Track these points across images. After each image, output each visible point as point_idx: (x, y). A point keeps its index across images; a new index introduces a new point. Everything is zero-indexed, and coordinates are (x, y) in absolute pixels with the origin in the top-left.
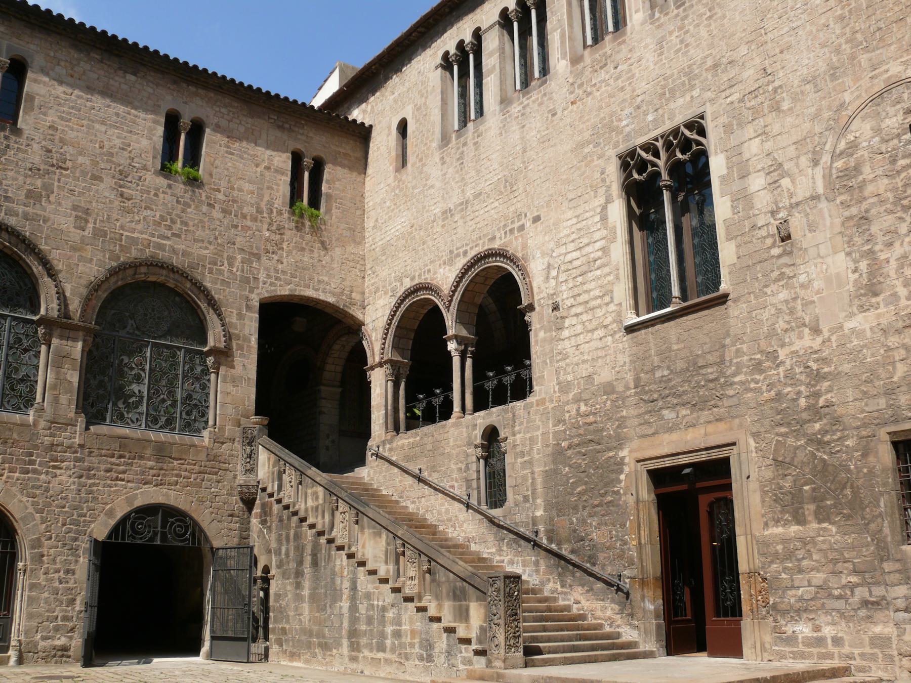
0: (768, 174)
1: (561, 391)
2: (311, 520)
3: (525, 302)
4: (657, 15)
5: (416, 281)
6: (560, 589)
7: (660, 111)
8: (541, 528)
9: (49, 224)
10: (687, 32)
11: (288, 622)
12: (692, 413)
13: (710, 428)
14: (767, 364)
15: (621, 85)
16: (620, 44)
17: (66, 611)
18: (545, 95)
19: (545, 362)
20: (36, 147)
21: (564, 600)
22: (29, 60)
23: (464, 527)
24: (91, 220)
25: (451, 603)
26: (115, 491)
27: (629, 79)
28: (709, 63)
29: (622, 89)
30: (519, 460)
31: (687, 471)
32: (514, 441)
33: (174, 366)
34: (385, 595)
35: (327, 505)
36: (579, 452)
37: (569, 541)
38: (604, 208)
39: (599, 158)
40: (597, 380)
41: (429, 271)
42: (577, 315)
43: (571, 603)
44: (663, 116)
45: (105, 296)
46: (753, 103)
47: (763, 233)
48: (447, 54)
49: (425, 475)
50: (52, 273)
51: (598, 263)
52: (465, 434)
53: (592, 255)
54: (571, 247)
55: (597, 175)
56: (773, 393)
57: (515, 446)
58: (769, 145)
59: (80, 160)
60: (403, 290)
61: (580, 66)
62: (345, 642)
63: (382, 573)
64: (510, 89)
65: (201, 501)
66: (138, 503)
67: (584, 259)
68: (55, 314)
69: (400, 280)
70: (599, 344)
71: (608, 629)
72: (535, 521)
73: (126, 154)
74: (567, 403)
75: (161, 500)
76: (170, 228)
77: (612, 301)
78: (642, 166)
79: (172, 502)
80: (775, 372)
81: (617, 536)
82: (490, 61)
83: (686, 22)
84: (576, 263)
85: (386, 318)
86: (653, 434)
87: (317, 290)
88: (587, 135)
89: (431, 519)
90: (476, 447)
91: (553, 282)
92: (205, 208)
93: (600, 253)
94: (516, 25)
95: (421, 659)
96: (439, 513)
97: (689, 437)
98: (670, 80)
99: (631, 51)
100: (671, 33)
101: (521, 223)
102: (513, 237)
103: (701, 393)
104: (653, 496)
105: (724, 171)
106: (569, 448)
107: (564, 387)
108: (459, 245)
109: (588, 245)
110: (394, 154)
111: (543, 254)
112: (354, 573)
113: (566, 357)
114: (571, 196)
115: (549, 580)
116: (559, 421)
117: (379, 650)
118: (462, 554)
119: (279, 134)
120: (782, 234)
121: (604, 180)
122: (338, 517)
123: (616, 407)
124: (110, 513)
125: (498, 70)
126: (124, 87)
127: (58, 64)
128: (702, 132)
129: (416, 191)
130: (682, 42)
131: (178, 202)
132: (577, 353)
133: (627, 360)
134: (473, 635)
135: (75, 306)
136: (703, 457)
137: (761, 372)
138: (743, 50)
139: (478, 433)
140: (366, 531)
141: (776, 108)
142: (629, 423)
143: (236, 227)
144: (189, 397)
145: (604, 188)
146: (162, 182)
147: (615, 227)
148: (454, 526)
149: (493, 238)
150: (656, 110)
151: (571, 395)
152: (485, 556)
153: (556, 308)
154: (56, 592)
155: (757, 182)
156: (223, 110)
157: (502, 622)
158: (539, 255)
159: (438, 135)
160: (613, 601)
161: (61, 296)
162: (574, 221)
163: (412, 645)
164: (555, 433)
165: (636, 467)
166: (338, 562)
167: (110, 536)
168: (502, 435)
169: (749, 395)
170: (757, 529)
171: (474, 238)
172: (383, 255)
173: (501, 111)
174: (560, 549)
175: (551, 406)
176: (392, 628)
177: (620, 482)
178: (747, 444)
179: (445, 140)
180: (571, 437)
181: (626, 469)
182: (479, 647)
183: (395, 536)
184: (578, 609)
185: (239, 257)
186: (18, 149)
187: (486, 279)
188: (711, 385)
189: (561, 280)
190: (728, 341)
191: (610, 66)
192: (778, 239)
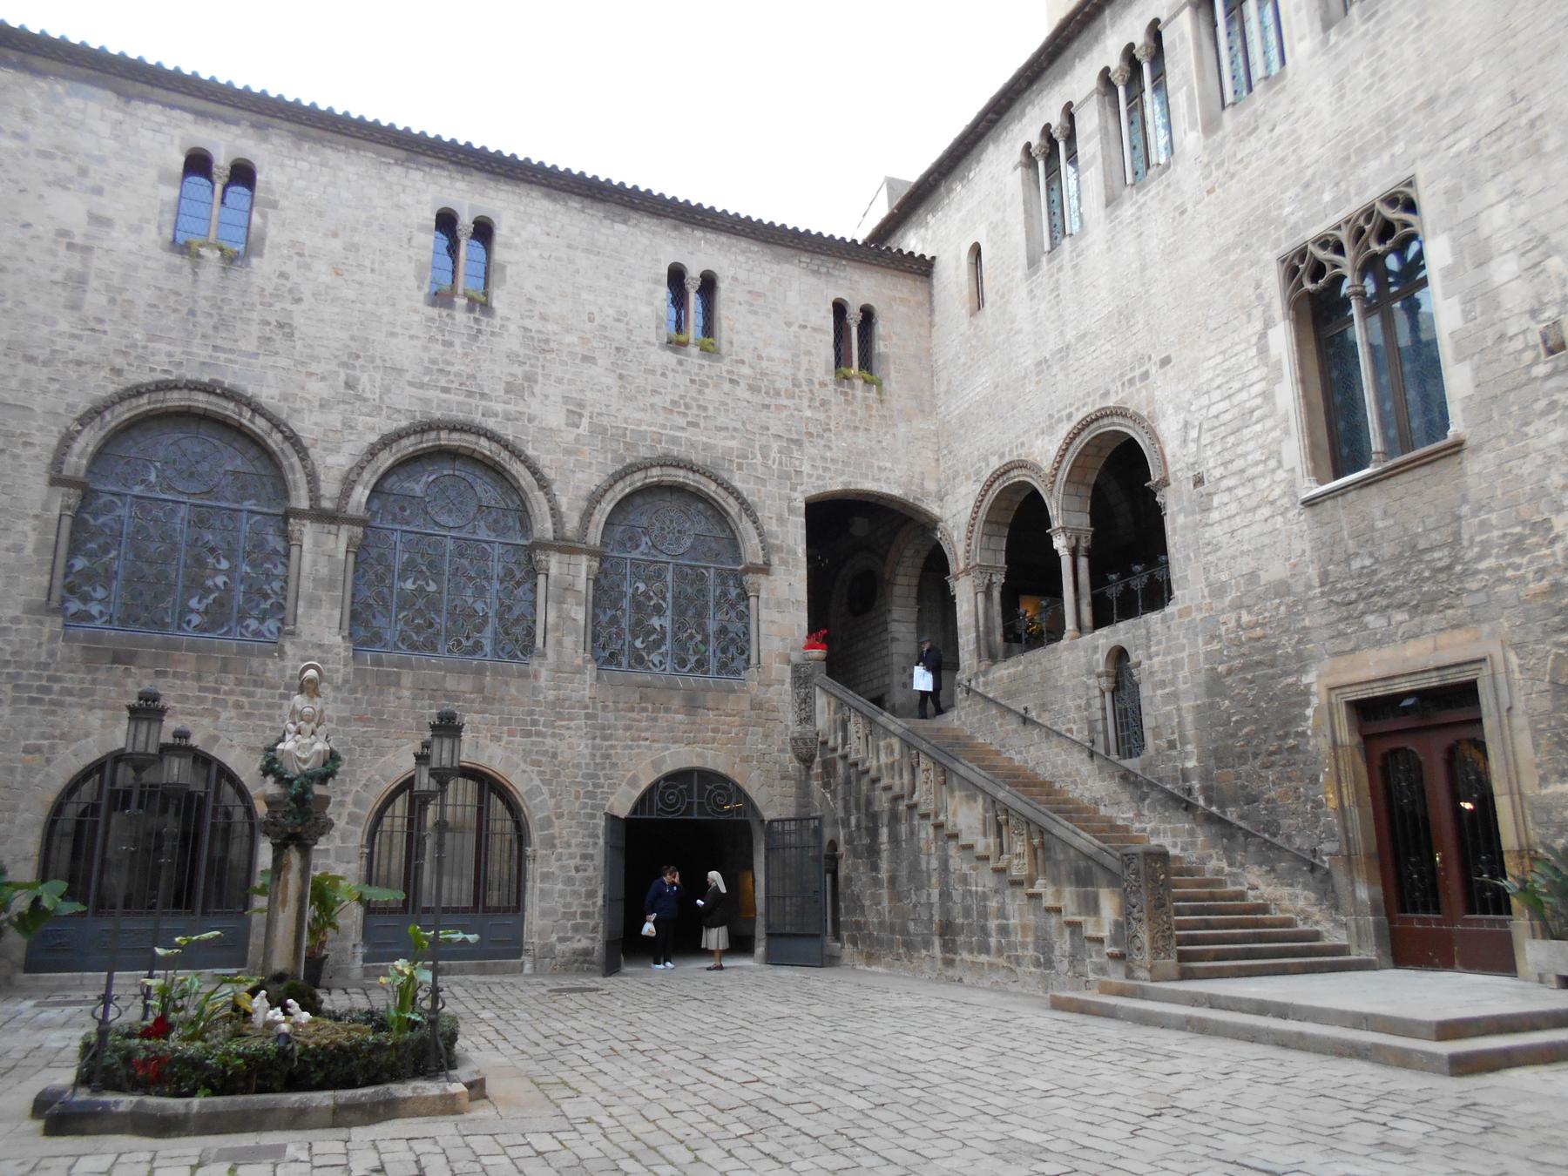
0: (1524, 254)
1: (1213, 595)
2: (885, 782)
3: (1155, 475)
4: (1333, 39)
5: (1007, 459)
6: (1227, 869)
7: (1343, 185)
8: (1196, 784)
9: (536, 423)
10: (1382, 56)
11: (863, 913)
12: (1411, 618)
13: (1443, 639)
14: (1533, 540)
15: (1281, 155)
16: (1276, 93)
17: (586, 906)
18: (1168, 185)
19: (1187, 558)
20: (513, 328)
21: (1234, 884)
22: (495, 221)
23: (1087, 782)
24: (586, 413)
25: (1073, 889)
26: (638, 755)
27: (1292, 144)
28: (1421, 97)
29: (1282, 161)
30: (1159, 692)
31: (1408, 702)
32: (1151, 666)
33: (702, 592)
34: (984, 881)
35: (905, 760)
36: (1244, 679)
37: (1235, 802)
38: (1263, 336)
39: (1252, 266)
40: (1264, 578)
41: (1023, 444)
42: (1229, 489)
43: (1244, 888)
44: (1347, 192)
45: (609, 508)
46: (1493, 150)
47: (1518, 344)
48: (1028, 146)
49: (1033, 715)
50: (544, 484)
51: (1257, 414)
52: (1083, 660)
53: (1248, 405)
54: (1216, 395)
55: (1250, 291)
56: (1545, 583)
58: (1522, 212)
59: (569, 339)
61: (1218, 136)
62: (937, 941)
63: (980, 849)
64: (1118, 183)
65: (746, 760)
66: (669, 767)
67: (1235, 411)
68: (550, 535)
69: (986, 459)
70: (1267, 527)
71: (1302, 927)
72: (1185, 775)
73: (622, 326)
74: (1223, 612)
75: (696, 763)
76: (685, 415)
77: (1280, 463)
78: (1318, 270)
79: (710, 765)
80: (1548, 552)
81: (1306, 796)
82: (1088, 146)
83: (1380, 41)
84: (1228, 416)
85: (969, 511)
86: (1353, 650)
87: (878, 480)
88: (1230, 237)
89: (1045, 773)
90: (1099, 676)
91: (1193, 447)
92: (727, 386)
93: (1259, 401)
94: (1121, 90)
95: (1037, 964)
96: (1054, 766)
97: (1408, 653)
98: (1357, 136)
99: (1293, 101)
100: (1356, 63)
101: (1143, 369)
102: (1133, 389)
103: (1425, 589)
104: (1357, 738)
105: (1448, 260)
106: (1229, 672)
107: (1218, 590)
108: (1060, 406)
109: (1240, 390)
110: (966, 292)
111: (1178, 409)
112: (945, 850)
113: (1217, 548)
114: (1212, 324)
115: (1211, 856)
116: (1213, 638)
117: (980, 952)
118: (1088, 820)
119: (812, 280)
120: (1550, 344)
121: (1260, 297)
122: (921, 777)
123: (1292, 613)
124: (633, 782)
125: (1100, 160)
126: (613, 240)
127: (530, 221)
128: (1411, 206)
129: (999, 339)
130: (1373, 73)
131: (692, 381)
132: (1233, 541)
133: (1307, 547)
134: (1105, 933)
135: (572, 524)
136: (1434, 681)
137: (1524, 552)
138: (1476, 69)
139: (1100, 659)
140: (957, 794)
141: (1535, 151)
142: (1313, 635)
143: (768, 407)
144: (723, 630)
145: (1261, 309)
146: (670, 358)
147: (1279, 362)
148: (1074, 782)
149: (1106, 394)
150: (1337, 184)
151: (1227, 600)
152: (1120, 822)
153: (1199, 481)
154: (569, 881)
155: (1504, 270)
156: (741, 258)
157: (1144, 916)
158: (1170, 410)
159: (1023, 261)
160: (1306, 886)
161: (555, 512)
162: (1219, 359)
163: (1024, 946)
165: (1329, 697)
166: (923, 835)
167: (635, 810)
168: (1133, 659)
169: (1505, 588)
170: (1530, 787)
171: (1080, 394)
172: (962, 426)
173: (1108, 216)
174: (1224, 813)
175: (1199, 616)
176: (997, 922)
177: (1306, 719)
178: (1506, 660)
179: (1033, 263)
180: (1230, 658)
181: (1315, 701)
182: (1115, 950)
183: (994, 801)
184: (1256, 898)
185: (775, 446)
186: (493, 334)
187: (1100, 449)
188: (1442, 576)
189: (1204, 442)
190: (1465, 510)
191: (1264, 129)
192: (1542, 349)
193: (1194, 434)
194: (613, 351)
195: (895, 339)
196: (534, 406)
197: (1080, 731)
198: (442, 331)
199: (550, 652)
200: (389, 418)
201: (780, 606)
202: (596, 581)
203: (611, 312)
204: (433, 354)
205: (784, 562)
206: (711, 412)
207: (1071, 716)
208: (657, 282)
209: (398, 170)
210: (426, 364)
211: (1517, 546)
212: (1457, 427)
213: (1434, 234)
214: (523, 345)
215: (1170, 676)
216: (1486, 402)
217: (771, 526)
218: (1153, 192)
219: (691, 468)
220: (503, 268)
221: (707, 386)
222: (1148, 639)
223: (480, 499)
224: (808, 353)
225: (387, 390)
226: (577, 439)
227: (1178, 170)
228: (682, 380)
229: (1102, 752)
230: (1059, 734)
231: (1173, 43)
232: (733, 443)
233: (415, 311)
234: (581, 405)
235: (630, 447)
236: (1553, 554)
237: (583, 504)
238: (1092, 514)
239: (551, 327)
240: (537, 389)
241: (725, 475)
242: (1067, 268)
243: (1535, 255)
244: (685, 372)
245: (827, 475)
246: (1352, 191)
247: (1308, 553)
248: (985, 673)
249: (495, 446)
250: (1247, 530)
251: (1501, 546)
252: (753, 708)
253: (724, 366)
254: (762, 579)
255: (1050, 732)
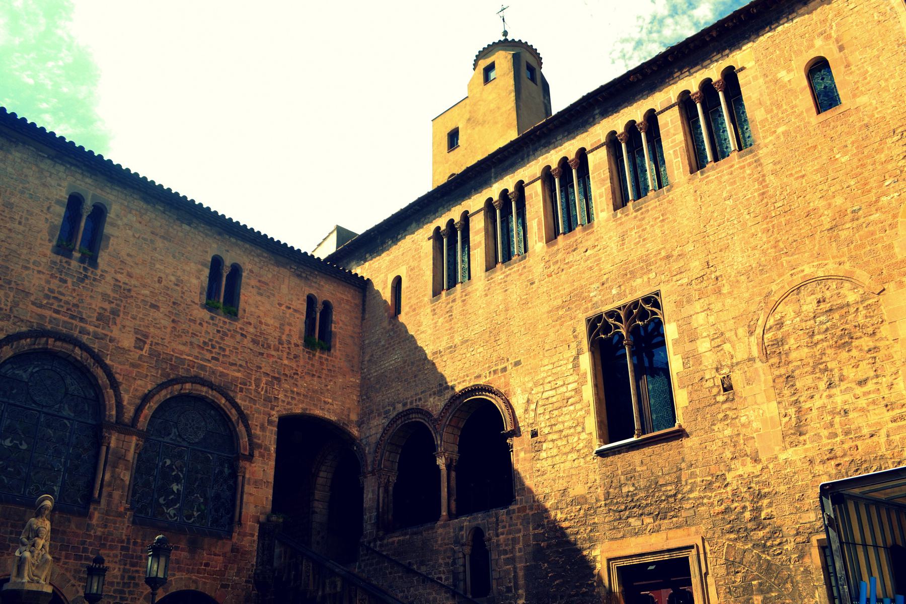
4: (619, 215)
5: (408, 407)
13: (671, 534)
14: (717, 484)
18: (525, 267)
20: (108, 278)
22: (108, 207)
27: (596, 261)
28: (663, 254)
29: (591, 268)
30: (502, 557)
32: (498, 541)
36: (557, 551)
38: (576, 358)
41: (420, 399)
42: (553, 441)
44: (625, 291)
46: (699, 287)
47: (710, 384)
51: (571, 401)
54: (547, 387)
57: (498, 545)
58: (712, 319)
60: (395, 413)
68: (114, 419)
69: (393, 405)
76: (211, 352)
77: (583, 428)
83: (643, 222)
84: (554, 399)
86: (623, 537)
87: (323, 409)
88: (559, 302)
91: (532, 414)
92: (238, 337)
100: (631, 229)
101: (503, 366)
102: (496, 376)
106: (549, 546)
119: (297, 281)
125: (483, 245)
126: (180, 234)
127: (130, 212)
128: (657, 305)
130: (640, 237)
131: (218, 331)
133: (598, 478)
137: (712, 490)
138: (690, 247)
142: (600, 528)
143: (262, 354)
146: (205, 314)
147: (586, 373)
155: (704, 346)
156: (256, 259)
162: (550, 367)
164: (534, 535)
173: (486, 277)
175: (531, 513)
179: (436, 293)
185: (264, 380)
186: (95, 280)
190: (683, 465)
193: (533, 406)
194: (171, 304)
195: (341, 324)
196: (115, 332)
197: (447, 579)
198: (61, 272)
199: (103, 501)
200: (14, 324)
201: (257, 483)
202: (139, 454)
203: (173, 278)
204: (52, 286)
205: (262, 456)
206: (227, 353)
207: (442, 569)
208: (204, 265)
209: (49, 161)
210: (46, 292)
211: (709, 486)
212: (681, 420)
213: (669, 321)
214: (114, 291)
215: (510, 547)
216: (695, 411)
217: (257, 431)
218: (515, 269)
219: (211, 386)
220: (108, 238)
221: (227, 335)
222: (497, 525)
223: (67, 389)
224: (290, 324)
225: (16, 304)
226: (140, 358)
227: (531, 260)
228: (212, 330)
229: (462, 592)
230: (432, 580)
231: (531, 195)
232: (239, 375)
233: (45, 256)
234: (146, 336)
235: (173, 367)
236: (727, 492)
237: (138, 401)
238: (460, 446)
239: (133, 282)
240: (118, 320)
241: (232, 394)
242: (459, 302)
243: (718, 341)
244: (214, 324)
245: (294, 402)
246: (627, 291)
247: (598, 481)
248: (382, 539)
249: (85, 354)
250: (562, 465)
251: (701, 486)
252: (232, 551)
253: (238, 325)
254: (247, 464)
255: (425, 579)
